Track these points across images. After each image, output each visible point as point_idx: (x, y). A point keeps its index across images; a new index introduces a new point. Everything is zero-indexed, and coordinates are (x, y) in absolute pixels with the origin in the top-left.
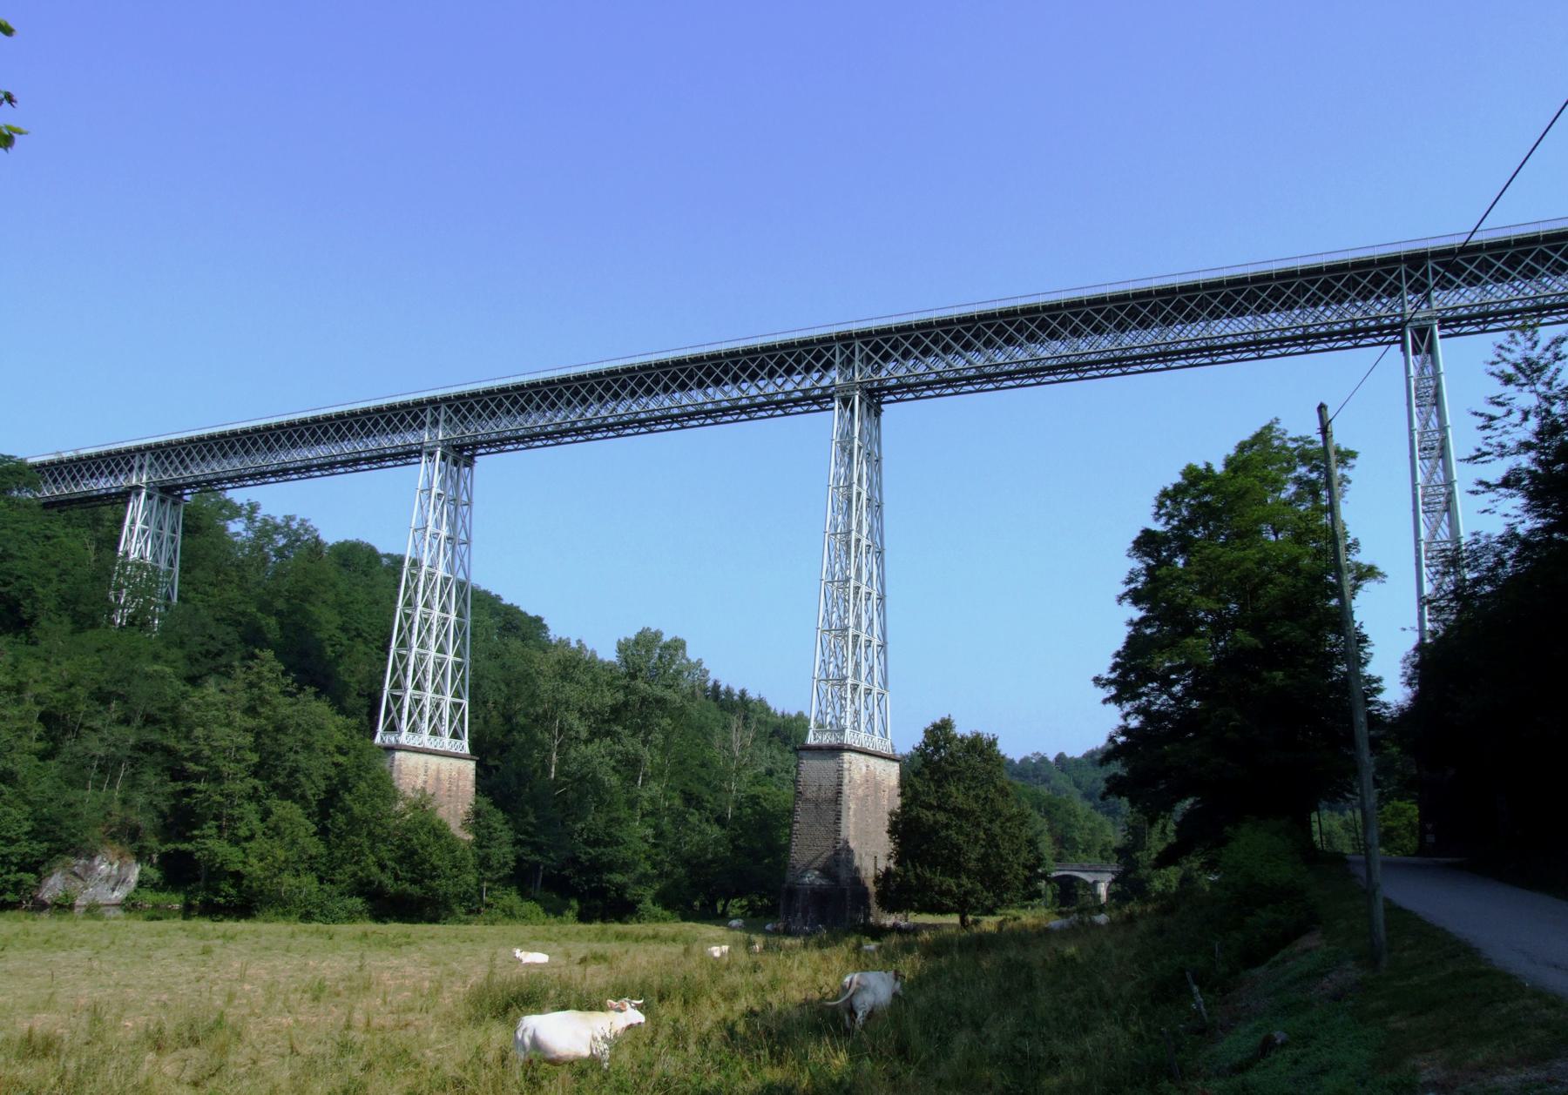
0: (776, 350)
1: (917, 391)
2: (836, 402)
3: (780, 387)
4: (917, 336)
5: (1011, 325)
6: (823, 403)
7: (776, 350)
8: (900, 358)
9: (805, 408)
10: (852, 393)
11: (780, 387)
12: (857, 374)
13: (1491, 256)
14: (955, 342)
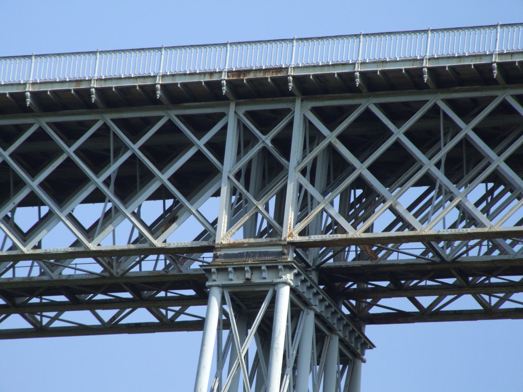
0: (153, 102)
1: (491, 289)
2: (215, 303)
3: (25, 237)
4: (368, 112)
5: (399, 120)
6: (168, 302)
7: (25, 110)
8: (439, 175)
9: (107, 315)
10: (268, 277)
11: (25, 237)
12: (290, 215)
13: (241, 349)
14: (492, 144)
